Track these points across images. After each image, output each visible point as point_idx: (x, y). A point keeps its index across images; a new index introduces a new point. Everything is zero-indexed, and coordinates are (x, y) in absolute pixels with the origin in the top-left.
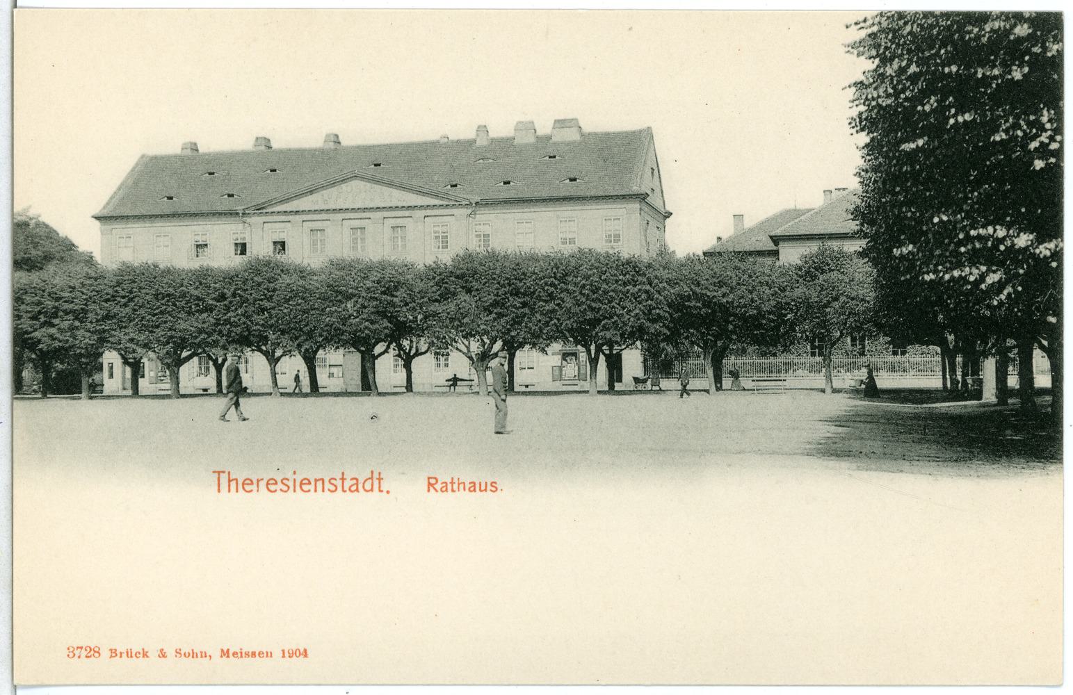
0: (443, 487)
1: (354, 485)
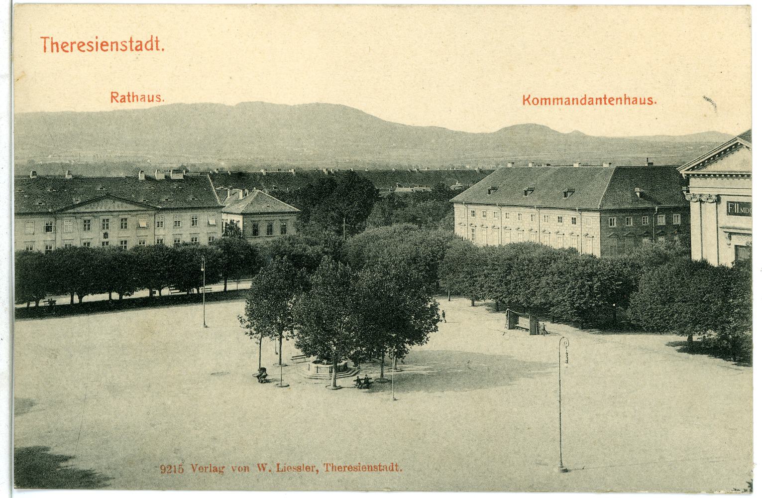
0: (122, 99)
1: (139, 45)
